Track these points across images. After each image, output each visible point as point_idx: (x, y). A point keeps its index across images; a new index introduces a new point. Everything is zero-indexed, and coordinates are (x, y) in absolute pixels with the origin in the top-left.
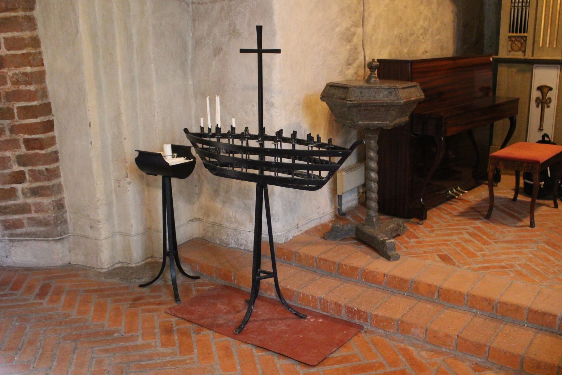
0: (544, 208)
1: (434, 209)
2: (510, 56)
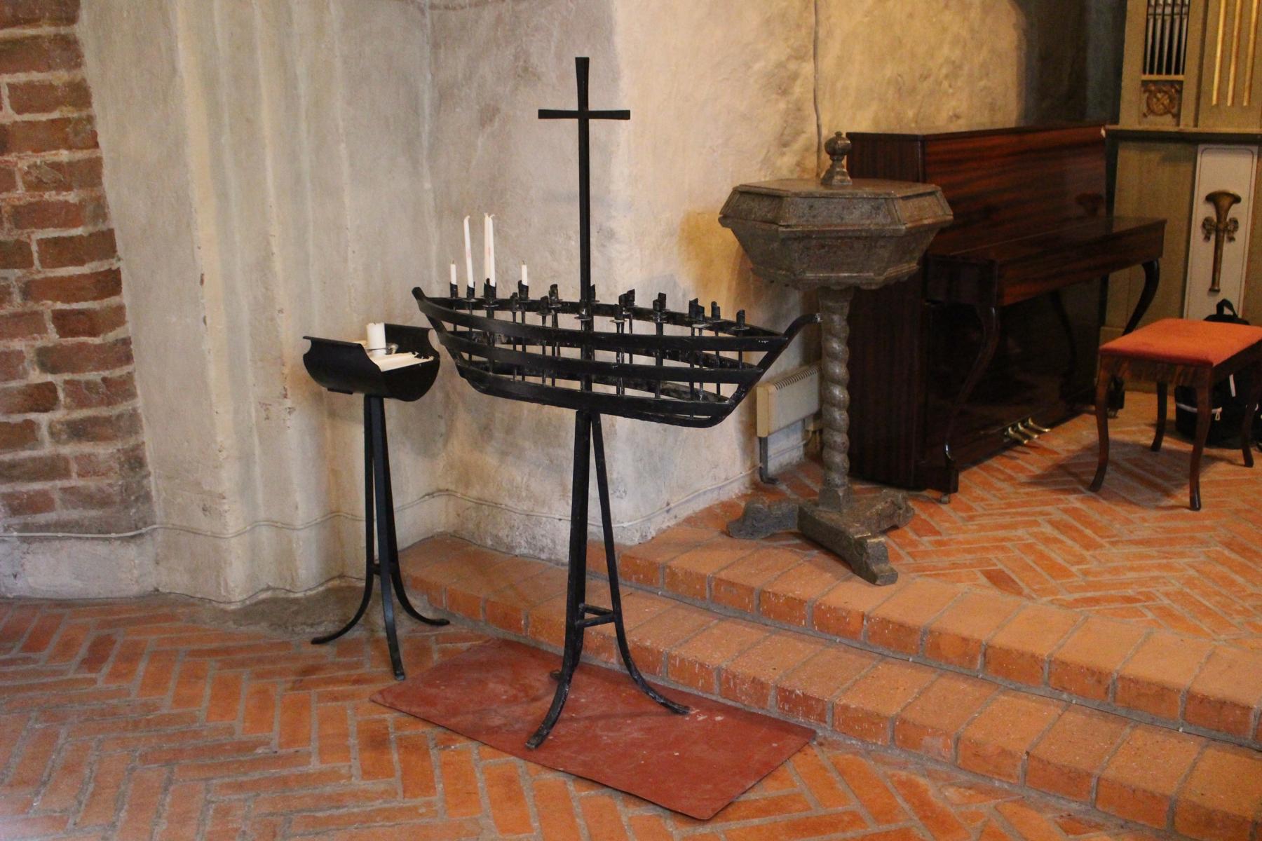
0: (1222, 467)
1: (975, 469)
2: (1145, 126)
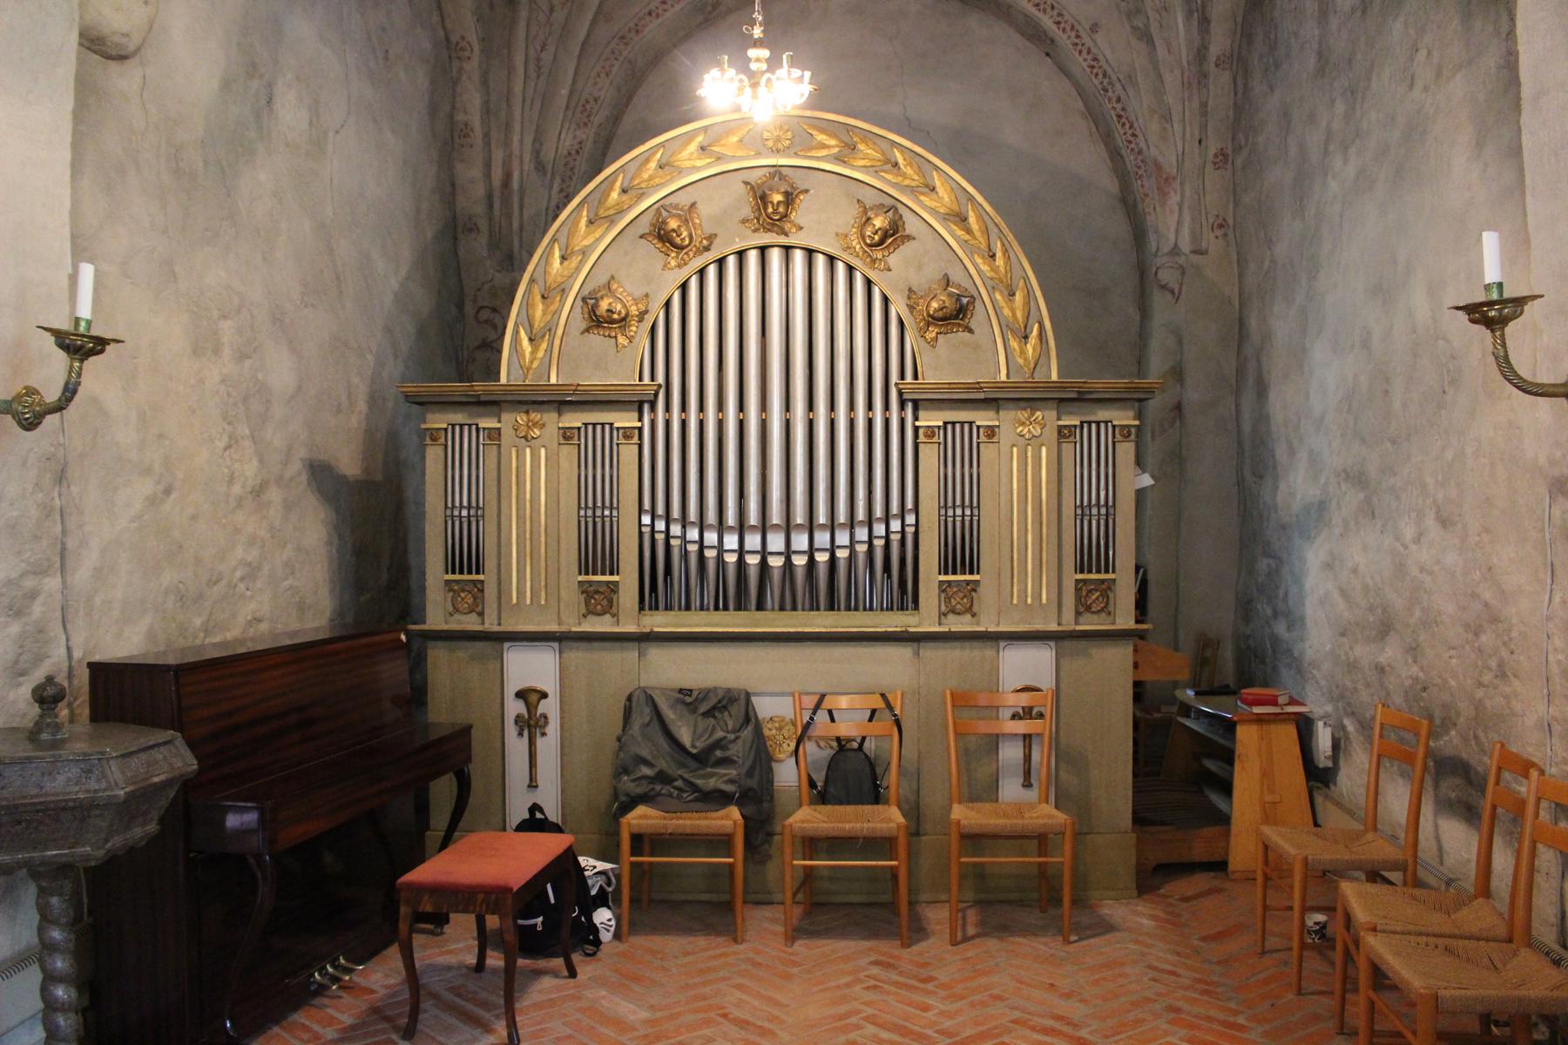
0: (547, 982)
1: (276, 1029)
2: (453, 626)
